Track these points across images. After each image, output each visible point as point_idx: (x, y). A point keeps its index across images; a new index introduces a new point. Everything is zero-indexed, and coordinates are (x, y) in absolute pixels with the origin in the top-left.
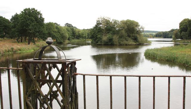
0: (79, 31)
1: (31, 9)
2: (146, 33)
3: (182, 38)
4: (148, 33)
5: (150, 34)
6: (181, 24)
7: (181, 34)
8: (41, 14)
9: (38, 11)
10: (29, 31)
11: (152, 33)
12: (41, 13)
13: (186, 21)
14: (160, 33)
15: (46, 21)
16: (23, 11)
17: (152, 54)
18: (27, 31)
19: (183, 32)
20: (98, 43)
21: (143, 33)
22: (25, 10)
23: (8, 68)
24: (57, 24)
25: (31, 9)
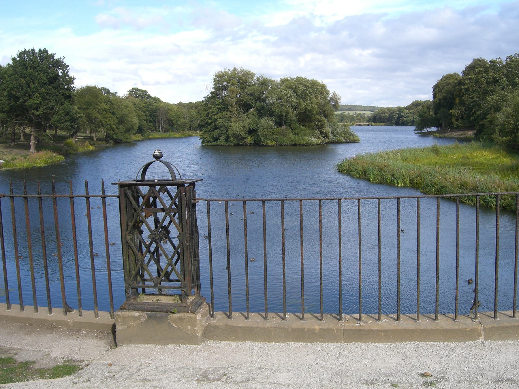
0: (168, 107)
1: (37, 51)
2: (345, 113)
3: (439, 126)
4: (352, 113)
5: (357, 116)
6: (437, 89)
7: (436, 113)
8: (65, 67)
9: (56, 57)
10: (34, 111)
11: (362, 112)
12: (66, 62)
13: (451, 81)
14: (383, 111)
15: (78, 84)
16: (16, 56)
17: (487, 148)
18: (28, 111)
19: (442, 109)
20: (218, 143)
21: (337, 113)
22: (22, 54)
23: (53, 194)
24: (109, 90)
25: (37, 51)
